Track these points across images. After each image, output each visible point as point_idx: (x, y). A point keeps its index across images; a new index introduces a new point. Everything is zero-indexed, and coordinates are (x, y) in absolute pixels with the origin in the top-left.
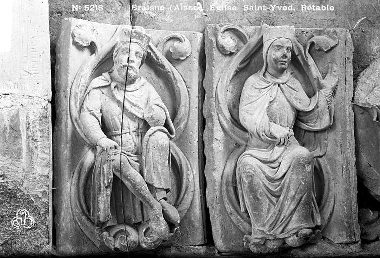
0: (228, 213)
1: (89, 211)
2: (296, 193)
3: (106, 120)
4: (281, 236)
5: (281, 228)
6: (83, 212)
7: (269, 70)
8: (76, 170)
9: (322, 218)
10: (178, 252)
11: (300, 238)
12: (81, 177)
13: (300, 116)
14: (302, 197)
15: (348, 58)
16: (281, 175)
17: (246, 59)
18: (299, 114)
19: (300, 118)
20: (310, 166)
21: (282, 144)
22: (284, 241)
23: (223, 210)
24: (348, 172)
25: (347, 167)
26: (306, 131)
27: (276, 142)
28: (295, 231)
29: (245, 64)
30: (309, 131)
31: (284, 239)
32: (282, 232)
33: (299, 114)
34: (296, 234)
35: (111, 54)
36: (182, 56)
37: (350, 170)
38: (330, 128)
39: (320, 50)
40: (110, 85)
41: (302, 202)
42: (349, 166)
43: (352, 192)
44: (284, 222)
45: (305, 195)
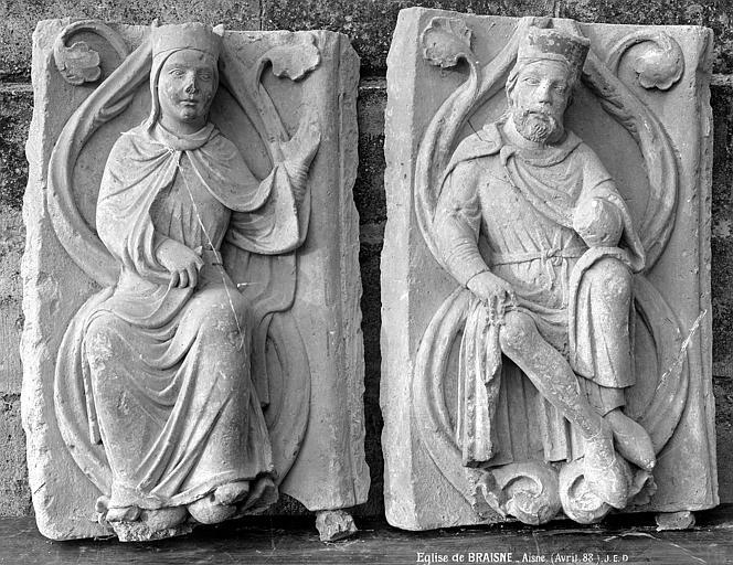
0: (64, 445)
1: (453, 426)
2: (208, 400)
3: (489, 228)
4: (178, 500)
5: (176, 483)
6: (440, 429)
7: (165, 119)
8: (426, 336)
9: (275, 455)
10: (353, 524)
11: (220, 505)
12: (436, 352)
13: (236, 220)
14: (222, 409)
15: (344, 94)
16: (175, 358)
17: (121, 96)
18: (235, 216)
19: (238, 224)
20: (242, 336)
21: (182, 285)
22: (187, 510)
23: (54, 443)
24: (341, 345)
25: (340, 333)
26: (251, 254)
27: (169, 281)
28: (207, 489)
29: (118, 107)
30: (259, 255)
31: (185, 507)
32: (179, 490)
33: (235, 216)
34: (211, 495)
35: (502, 85)
36: (662, 82)
37: (347, 340)
38: (300, 250)
39: (284, 77)
40: (498, 152)
41: (222, 420)
42: (346, 333)
43: (349, 390)
44: (185, 462)
45: (229, 403)
